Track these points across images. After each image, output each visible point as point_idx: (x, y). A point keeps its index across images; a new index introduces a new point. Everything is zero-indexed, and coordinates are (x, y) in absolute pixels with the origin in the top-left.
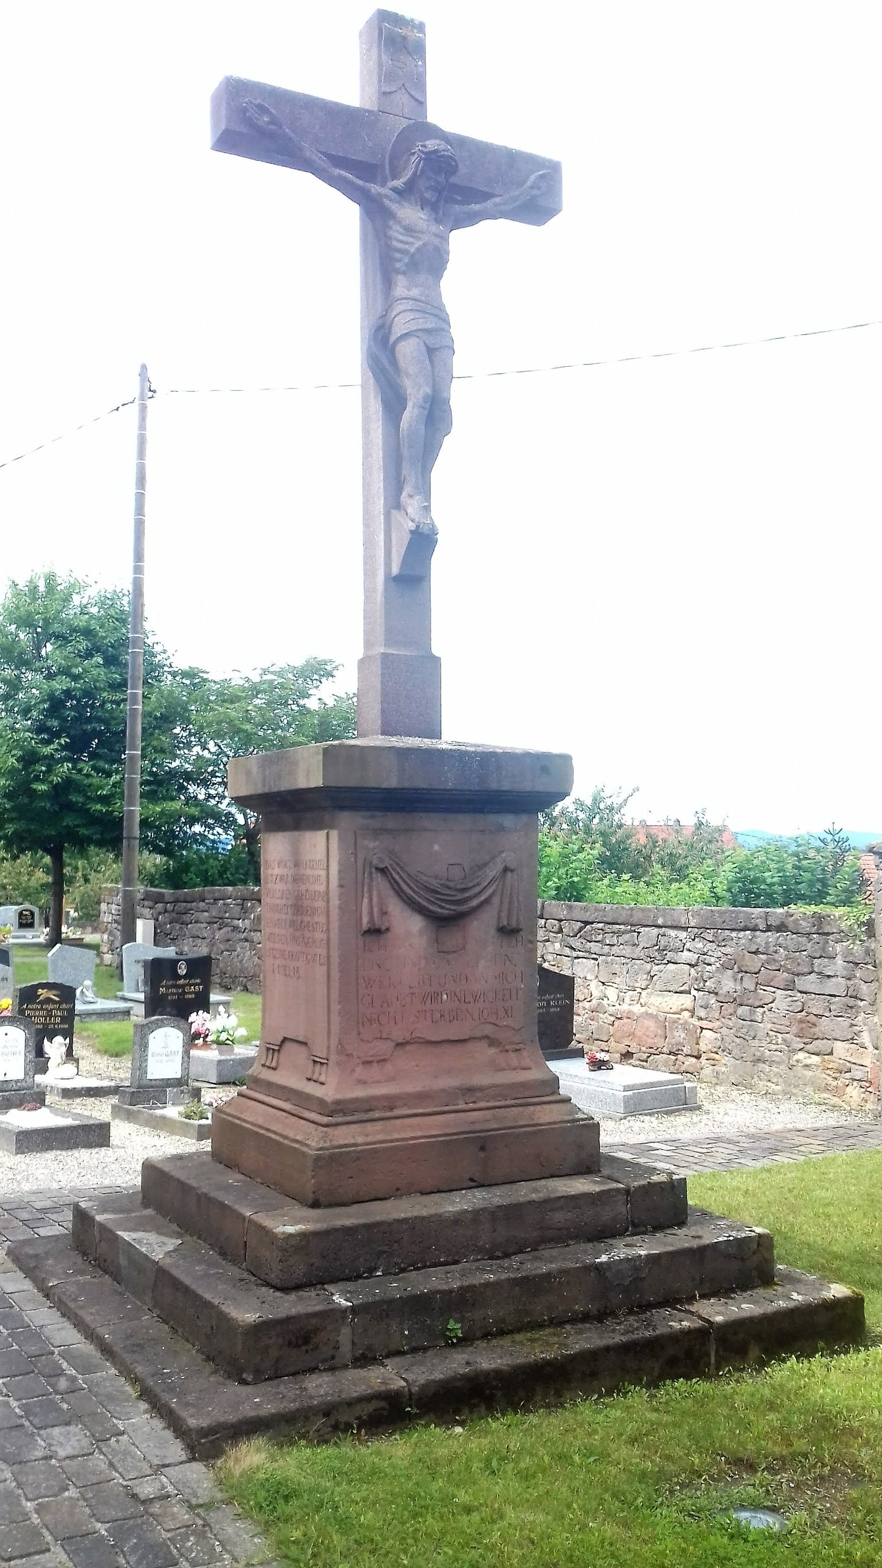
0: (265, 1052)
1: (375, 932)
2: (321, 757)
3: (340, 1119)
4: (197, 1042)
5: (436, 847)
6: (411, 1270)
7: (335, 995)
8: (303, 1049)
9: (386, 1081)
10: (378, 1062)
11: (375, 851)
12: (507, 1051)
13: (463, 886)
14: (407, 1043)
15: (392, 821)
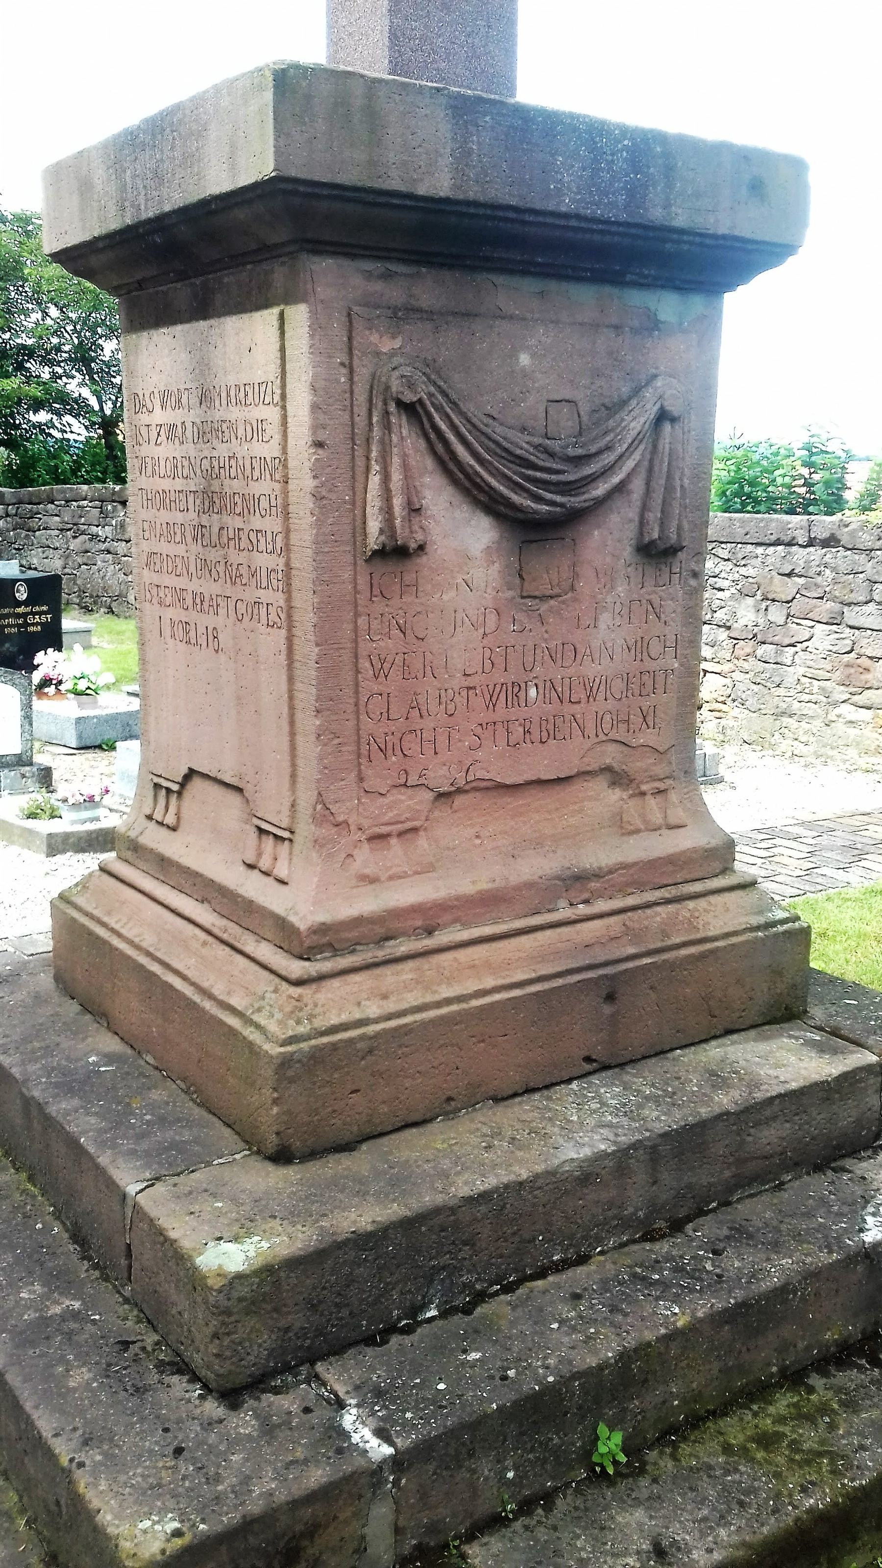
0: (151, 793)
1: (396, 553)
2: (269, 96)
3: (326, 966)
4: (46, 690)
5: (524, 359)
6: (496, 1294)
7: (307, 694)
8: (234, 799)
9: (417, 873)
10: (400, 834)
11: (397, 360)
12: (643, 794)
13: (580, 452)
14: (460, 791)
15: (429, 290)
